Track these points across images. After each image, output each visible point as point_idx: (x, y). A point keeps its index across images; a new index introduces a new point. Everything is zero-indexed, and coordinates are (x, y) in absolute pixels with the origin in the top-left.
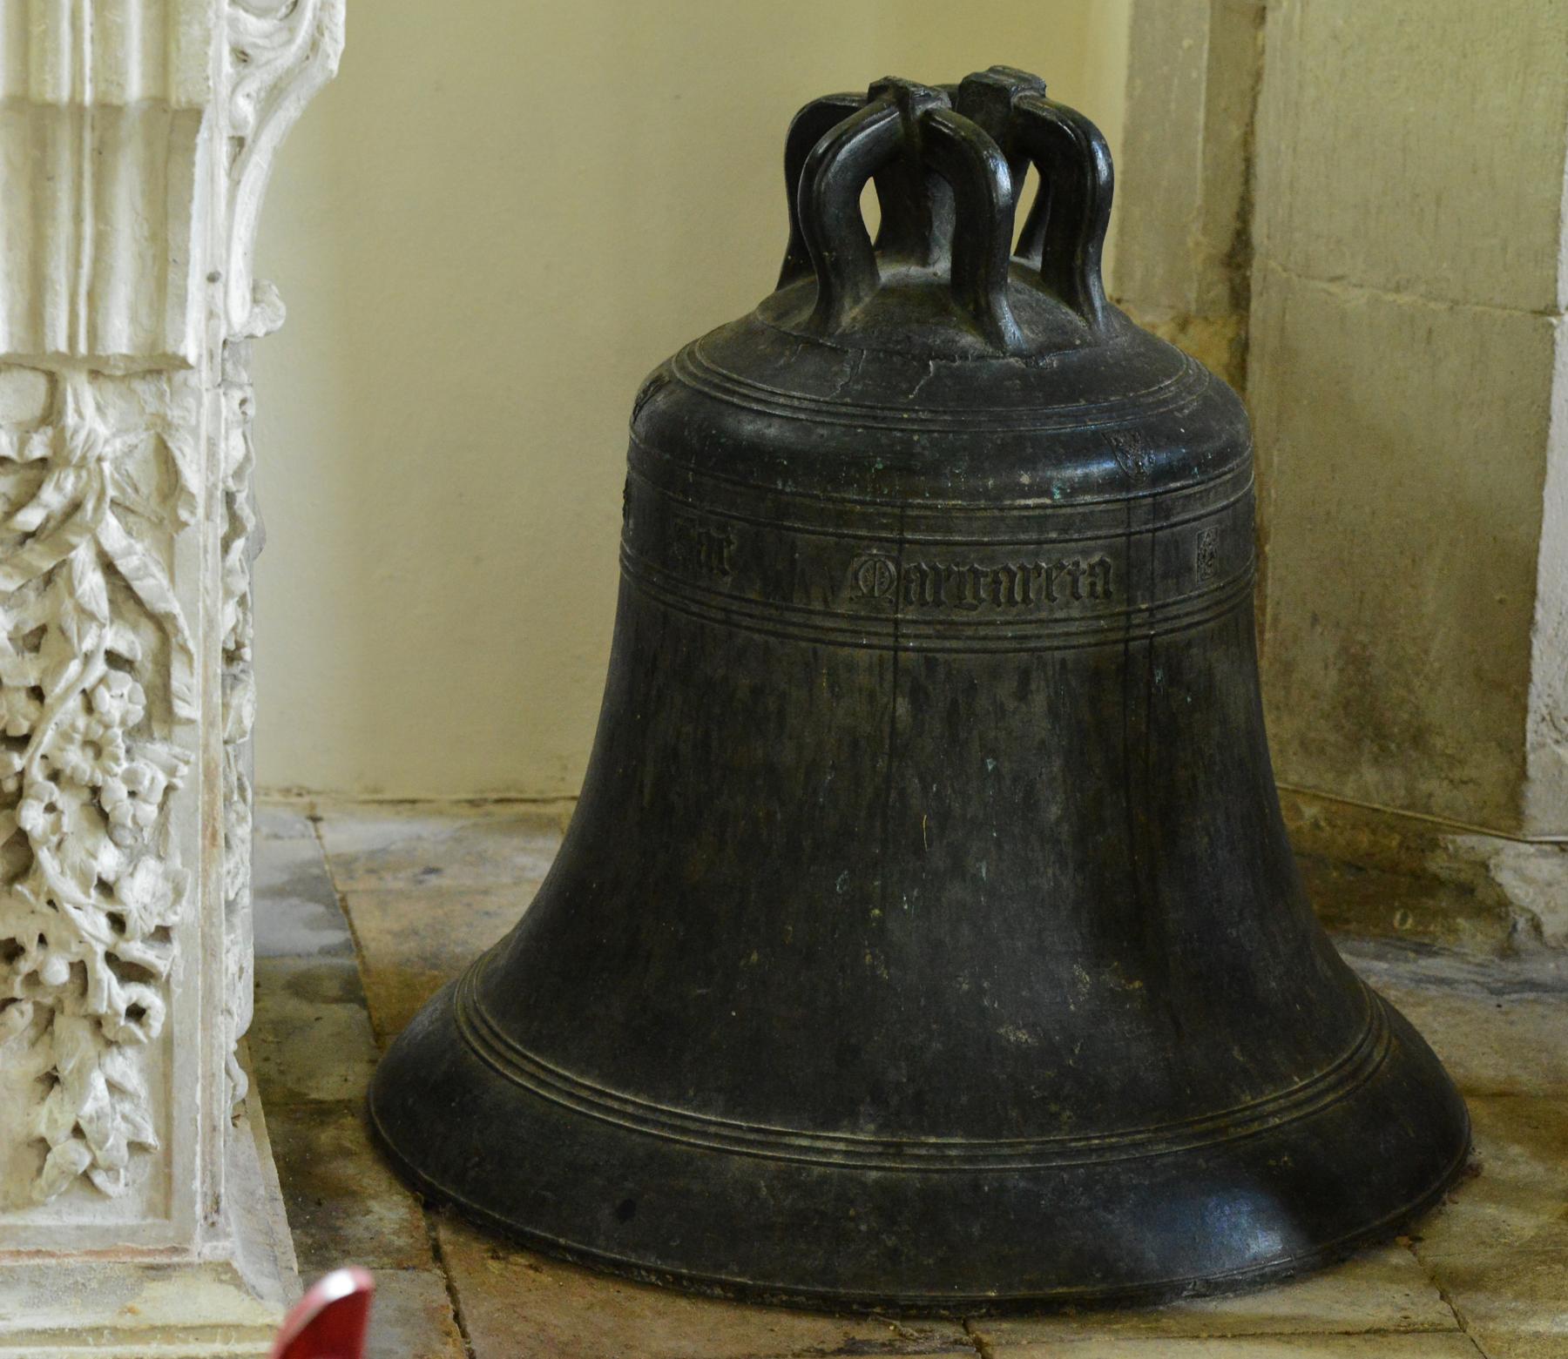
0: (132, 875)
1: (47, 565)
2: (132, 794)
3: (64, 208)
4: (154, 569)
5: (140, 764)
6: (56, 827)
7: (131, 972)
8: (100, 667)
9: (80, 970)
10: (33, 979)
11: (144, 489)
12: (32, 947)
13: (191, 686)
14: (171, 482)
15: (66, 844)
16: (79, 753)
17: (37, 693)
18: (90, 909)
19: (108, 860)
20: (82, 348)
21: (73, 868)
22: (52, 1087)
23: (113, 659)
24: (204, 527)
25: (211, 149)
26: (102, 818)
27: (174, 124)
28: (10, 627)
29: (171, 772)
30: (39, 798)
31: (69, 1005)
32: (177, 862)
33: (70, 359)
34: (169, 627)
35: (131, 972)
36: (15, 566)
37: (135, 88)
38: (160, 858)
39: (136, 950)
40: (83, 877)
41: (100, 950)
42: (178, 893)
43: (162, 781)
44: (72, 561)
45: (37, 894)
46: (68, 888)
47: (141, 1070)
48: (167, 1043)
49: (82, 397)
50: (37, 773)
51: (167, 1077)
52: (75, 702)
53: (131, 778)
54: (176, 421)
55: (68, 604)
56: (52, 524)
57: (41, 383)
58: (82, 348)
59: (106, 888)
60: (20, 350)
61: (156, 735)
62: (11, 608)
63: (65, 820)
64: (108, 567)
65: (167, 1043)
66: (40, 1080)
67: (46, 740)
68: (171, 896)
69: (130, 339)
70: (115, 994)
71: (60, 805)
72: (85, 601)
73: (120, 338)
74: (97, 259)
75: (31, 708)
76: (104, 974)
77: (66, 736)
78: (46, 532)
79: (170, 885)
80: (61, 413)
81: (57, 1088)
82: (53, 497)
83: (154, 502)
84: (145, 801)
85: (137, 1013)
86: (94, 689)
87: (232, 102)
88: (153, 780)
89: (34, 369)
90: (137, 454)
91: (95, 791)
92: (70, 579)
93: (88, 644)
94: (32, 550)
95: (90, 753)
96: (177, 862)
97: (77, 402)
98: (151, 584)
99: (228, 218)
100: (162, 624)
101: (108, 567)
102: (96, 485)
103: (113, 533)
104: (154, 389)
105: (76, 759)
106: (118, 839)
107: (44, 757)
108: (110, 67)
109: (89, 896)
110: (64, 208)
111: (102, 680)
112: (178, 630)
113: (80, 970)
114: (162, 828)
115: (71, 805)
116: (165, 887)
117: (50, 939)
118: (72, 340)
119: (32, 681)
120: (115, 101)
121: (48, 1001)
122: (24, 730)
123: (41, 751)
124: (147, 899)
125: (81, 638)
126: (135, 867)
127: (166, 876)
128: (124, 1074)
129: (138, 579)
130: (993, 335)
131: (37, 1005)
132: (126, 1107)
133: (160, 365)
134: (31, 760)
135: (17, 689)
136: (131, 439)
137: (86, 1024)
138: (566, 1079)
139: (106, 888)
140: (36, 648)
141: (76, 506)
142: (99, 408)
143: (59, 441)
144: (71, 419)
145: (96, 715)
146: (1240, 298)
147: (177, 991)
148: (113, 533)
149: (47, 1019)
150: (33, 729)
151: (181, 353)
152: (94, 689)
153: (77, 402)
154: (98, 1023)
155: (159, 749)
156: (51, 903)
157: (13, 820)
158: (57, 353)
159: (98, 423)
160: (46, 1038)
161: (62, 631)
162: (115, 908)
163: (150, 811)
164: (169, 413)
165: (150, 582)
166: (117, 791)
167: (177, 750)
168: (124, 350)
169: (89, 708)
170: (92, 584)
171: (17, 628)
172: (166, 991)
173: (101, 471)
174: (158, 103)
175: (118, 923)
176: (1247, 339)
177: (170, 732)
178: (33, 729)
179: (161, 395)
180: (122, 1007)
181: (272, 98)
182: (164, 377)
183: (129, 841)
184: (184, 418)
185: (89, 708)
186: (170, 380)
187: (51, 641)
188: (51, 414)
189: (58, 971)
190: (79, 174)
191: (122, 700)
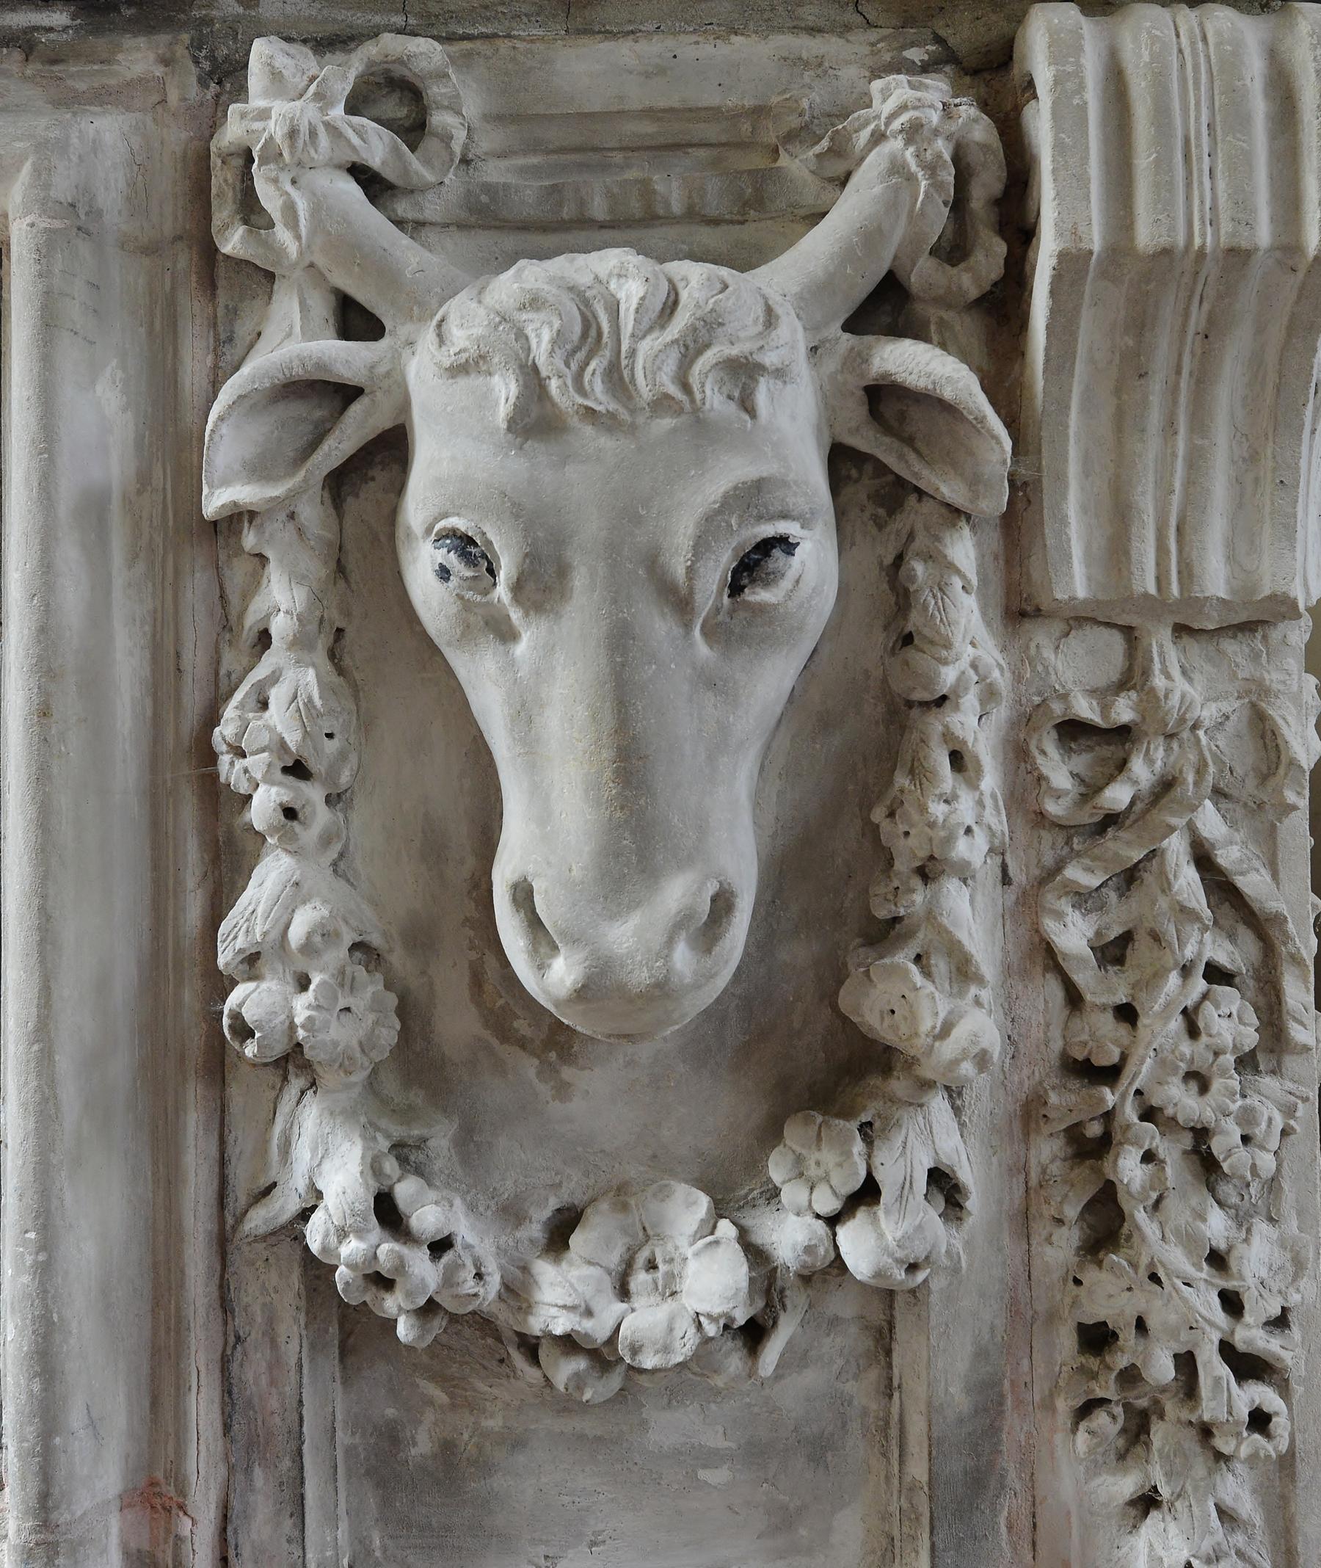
0: (1246, 1240)
1: (1137, 855)
2: (1246, 1139)
3: (1155, 418)
4: (1257, 864)
5: (1253, 1100)
6: (1157, 1181)
7: (1248, 1366)
8: (1200, 985)
9: (1186, 1363)
10: (1130, 1377)
11: (1239, 771)
12: (1128, 1336)
15: (1165, 1203)
16: (1182, 1087)
17: (1127, 1014)
18: (1202, 1285)
19: (1217, 1226)
20: (1175, 589)
21: (1177, 1232)
22: (1145, 1514)
23: (1216, 974)
26: (1207, 1166)
28: (1090, 934)
29: (1289, 1111)
30: (1137, 1143)
31: (1171, 1408)
32: (1292, 1225)
33: (1155, 606)
34: (1274, 933)
35: (1248, 1366)
36: (1094, 859)
37: (1263, 235)
38: (1271, 1220)
39: (1251, 1336)
40: (1189, 1240)
41: (1216, 1337)
42: (1299, 1265)
43: (1279, 1123)
44: (1163, 851)
45: (1134, 1266)
46: (1177, 1259)
47: (1254, 1491)
48: (1287, 1463)
49: (1163, 648)
50: (1130, 1113)
51: (1285, 1500)
52: (1176, 1023)
53: (1247, 1117)
54: (1275, 686)
55: (1163, 903)
56: (1139, 806)
57: (1116, 641)
58: (1175, 589)
59: (1217, 1260)
60: (1101, 597)
61: (1261, 1067)
62: (1089, 911)
63: (1169, 1170)
64: (1203, 859)
65: (1287, 1463)
66: (1132, 1503)
67: (1142, 1071)
68: (1290, 1269)
69: (1228, 582)
70: (1227, 1397)
71: (1162, 1153)
72: (1183, 897)
73: (1216, 580)
74: (1189, 483)
75: (1123, 1030)
76: (1213, 1368)
77: (1165, 1065)
78: (1133, 817)
79: (1288, 1256)
80: (1146, 673)
81: (1154, 1515)
82: (1142, 771)
83: (1251, 783)
84: (1262, 1148)
85: (1260, 1421)
86: (1197, 1006)
88: (1270, 1119)
89: (1108, 625)
90: (1229, 726)
91: (1201, 1134)
92: (1163, 874)
93: (1190, 951)
94: (1115, 839)
95: (1194, 1086)
96: (1292, 1225)
97: (1163, 662)
98: (1254, 883)
101: (1203, 859)
102: (1192, 757)
103: (1210, 821)
104: (1247, 650)
105: (1181, 1100)
106: (1221, 1196)
107: (1138, 1092)
108: (1244, 217)
109: (1201, 1270)
110: (1155, 418)
111: (1205, 996)
112: (1287, 937)
113: (1186, 1363)
114: (1273, 1185)
115: (1172, 1151)
116: (1280, 1257)
117: (1151, 1323)
118: (1161, 580)
119: (1122, 998)
120: (1244, 244)
121: (1143, 1403)
122: (1115, 1058)
123: (1136, 1086)
124: (1264, 1273)
125: (1182, 944)
126: (1249, 1231)
127: (1282, 1244)
128: (1237, 1498)
129: (1242, 874)
131: (1127, 1407)
132: (1239, 1539)
134: (1123, 1097)
135: (1103, 1008)
136: (1226, 707)
137: (1192, 1433)
139: (1217, 1260)
140: (1120, 961)
141: (1166, 785)
142: (1184, 672)
143: (1151, 701)
144: (1159, 682)
145: (1204, 1039)
147: (1298, 1390)
148: (1210, 821)
149: (1138, 1428)
150: (1124, 1057)
151: (1292, 595)
152: (1197, 1006)
153: (1163, 662)
154: (1206, 1431)
155: (1268, 1083)
156: (1154, 1278)
157: (1098, 1171)
158: (1146, 595)
159: (1188, 685)
160: (1139, 1449)
161: (1156, 937)
162: (1231, 1284)
163: (1267, 1162)
164: (1266, 676)
165: (1253, 877)
166: (1225, 1143)
167: (1289, 1085)
168: (1222, 595)
169: (1193, 1031)
170: (1188, 882)
171: (1098, 934)
172: (1284, 1389)
173: (1198, 740)
175: (1232, 1303)
177: (1279, 1063)
178: (1124, 1057)
179: (1255, 657)
180: (1243, 1413)
182: (1259, 635)
183: (1234, 1199)
184: (1284, 682)
185: (1193, 1031)
186: (1265, 637)
187: (1141, 950)
188: (1133, 676)
189: (1162, 1369)
190: (1175, 390)
191: (1231, 1021)
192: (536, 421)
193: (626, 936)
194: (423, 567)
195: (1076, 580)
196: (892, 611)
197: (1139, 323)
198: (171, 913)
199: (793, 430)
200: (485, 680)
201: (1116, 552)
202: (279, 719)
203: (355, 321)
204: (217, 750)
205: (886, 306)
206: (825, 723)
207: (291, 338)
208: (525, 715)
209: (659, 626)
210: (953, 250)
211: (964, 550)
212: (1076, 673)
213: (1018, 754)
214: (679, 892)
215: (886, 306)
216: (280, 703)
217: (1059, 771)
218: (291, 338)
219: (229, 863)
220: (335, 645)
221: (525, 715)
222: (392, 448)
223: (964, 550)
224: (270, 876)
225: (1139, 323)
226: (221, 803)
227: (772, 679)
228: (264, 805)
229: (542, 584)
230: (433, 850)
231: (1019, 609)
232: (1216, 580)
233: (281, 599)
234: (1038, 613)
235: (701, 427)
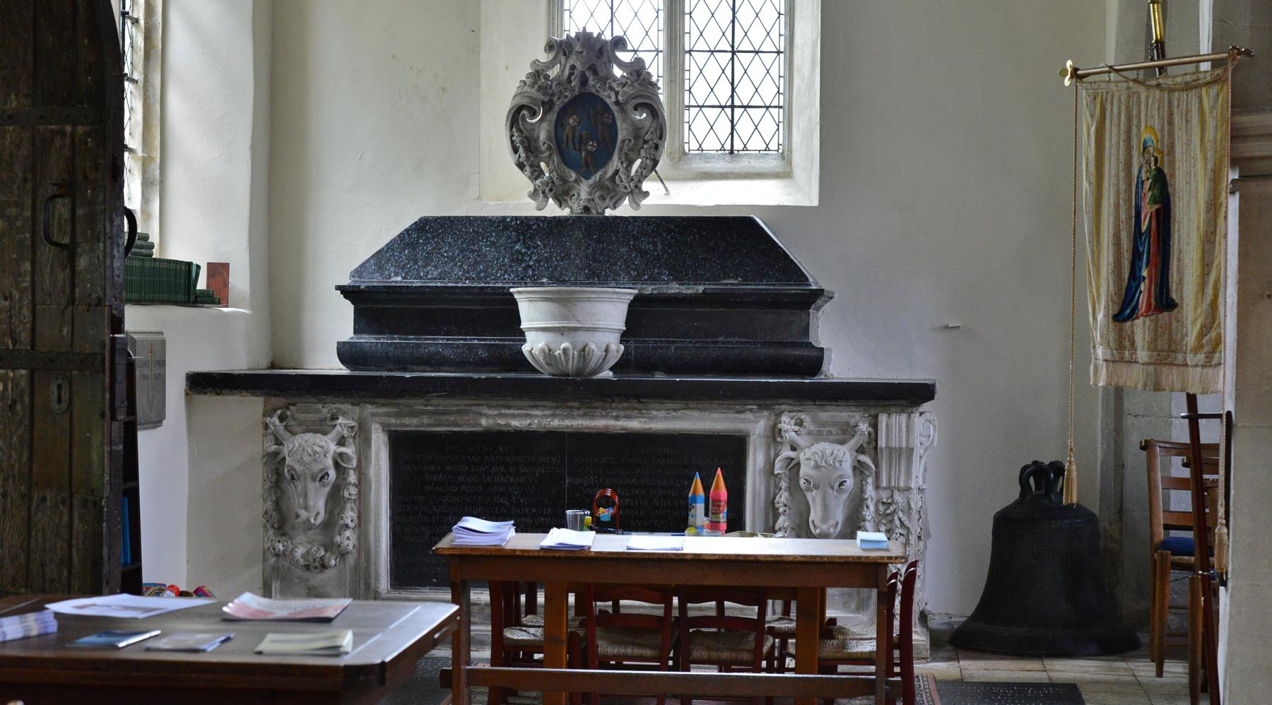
13: (913, 539)
14: (910, 508)
24: (915, 516)
25: (916, 458)
27: (910, 451)
49: (896, 493)
82: (892, 508)
87: (919, 450)
98: (907, 523)
99: (918, 468)
100: (908, 529)
108: (901, 442)
130: (1051, 500)
133: (908, 489)
138: (1119, 113)
146: (1121, 519)
148: (901, 514)
159: (898, 497)
170: (897, 522)
174: (887, 447)
176: (511, 128)
181: (926, 450)
188: (892, 496)
192: (817, 467)
193: (824, 527)
194: (802, 482)
195: (884, 484)
196: (861, 490)
197: (890, 454)
198: (1221, 511)
199: (847, 468)
200: (809, 496)
201: (889, 481)
202: (783, 499)
203: (793, 449)
204: (128, 141)
205: (861, 450)
206: (853, 500)
207: (786, 453)
208: (814, 500)
209: (830, 491)
210: (868, 443)
211: (870, 480)
212: (885, 496)
213: (876, 506)
214: (832, 522)
215: (861, 450)
216: (783, 497)
217: (882, 508)
218: (786, 453)
219: (776, 516)
220: (789, 489)
221: (814, 500)
222: (798, 465)
223: (870, 480)
224: (781, 519)
225: (890, 454)
226: (775, 510)
227: (845, 496)
228: (781, 510)
229: (816, 487)
230: (801, 515)
231: (877, 487)
232: (902, 484)
233: (784, 484)
234: (1136, 362)
235: (835, 468)
